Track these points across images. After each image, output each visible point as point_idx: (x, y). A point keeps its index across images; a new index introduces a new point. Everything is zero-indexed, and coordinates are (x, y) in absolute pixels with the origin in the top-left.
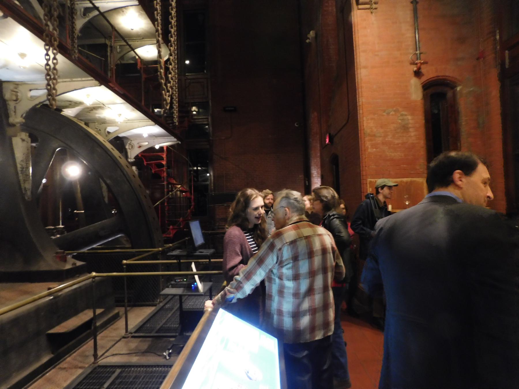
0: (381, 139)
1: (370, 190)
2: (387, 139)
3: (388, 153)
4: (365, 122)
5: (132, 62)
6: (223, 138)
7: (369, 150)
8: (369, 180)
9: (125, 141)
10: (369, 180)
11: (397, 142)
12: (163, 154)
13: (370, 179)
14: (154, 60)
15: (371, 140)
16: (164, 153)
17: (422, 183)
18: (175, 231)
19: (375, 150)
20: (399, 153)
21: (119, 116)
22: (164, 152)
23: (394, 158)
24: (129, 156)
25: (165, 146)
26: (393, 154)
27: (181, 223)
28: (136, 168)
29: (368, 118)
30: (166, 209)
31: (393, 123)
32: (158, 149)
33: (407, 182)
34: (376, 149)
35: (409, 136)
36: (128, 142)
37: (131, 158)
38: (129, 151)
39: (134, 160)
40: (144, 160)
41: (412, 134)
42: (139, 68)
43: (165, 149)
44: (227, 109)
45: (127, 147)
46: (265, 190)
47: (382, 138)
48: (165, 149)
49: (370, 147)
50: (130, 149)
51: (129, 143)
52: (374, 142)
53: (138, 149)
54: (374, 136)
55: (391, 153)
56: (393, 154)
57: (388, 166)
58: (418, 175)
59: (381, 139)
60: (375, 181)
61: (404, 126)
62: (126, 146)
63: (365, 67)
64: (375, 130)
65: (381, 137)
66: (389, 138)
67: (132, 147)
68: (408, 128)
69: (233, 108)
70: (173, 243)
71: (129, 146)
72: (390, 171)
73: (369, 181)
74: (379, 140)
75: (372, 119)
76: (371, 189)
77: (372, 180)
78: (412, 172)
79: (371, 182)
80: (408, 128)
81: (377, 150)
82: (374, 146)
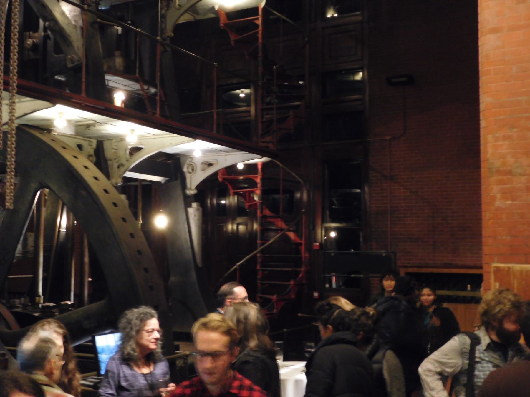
0: (523, 179)
4: (489, 145)
5: (212, 15)
6: (388, 138)
7: (498, 203)
9: (182, 159)
12: (256, 177)
13: (499, 262)
14: (240, 9)
15: (501, 182)
16: (257, 175)
19: (509, 202)
21: (132, 133)
24: (188, 185)
25: (260, 162)
28: (197, 205)
29: (497, 135)
30: (259, 277)
32: (242, 170)
34: (513, 200)
37: (190, 189)
38: (188, 176)
40: (230, 187)
42: (222, 25)
43: (259, 167)
44: (394, 80)
45: (185, 170)
46: (136, 308)
47: (526, 177)
48: (259, 167)
49: (499, 196)
50: (190, 173)
51: (188, 162)
52: (509, 186)
54: (510, 173)
59: (523, 179)
60: (507, 269)
62: (183, 168)
63: (495, 31)
64: (510, 160)
65: (523, 175)
67: (193, 170)
69: (405, 79)
70: (168, 355)
71: (188, 168)
73: (495, 267)
75: (505, 138)
76: (497, 285)
79: (498, 270)
81: (515, 202)
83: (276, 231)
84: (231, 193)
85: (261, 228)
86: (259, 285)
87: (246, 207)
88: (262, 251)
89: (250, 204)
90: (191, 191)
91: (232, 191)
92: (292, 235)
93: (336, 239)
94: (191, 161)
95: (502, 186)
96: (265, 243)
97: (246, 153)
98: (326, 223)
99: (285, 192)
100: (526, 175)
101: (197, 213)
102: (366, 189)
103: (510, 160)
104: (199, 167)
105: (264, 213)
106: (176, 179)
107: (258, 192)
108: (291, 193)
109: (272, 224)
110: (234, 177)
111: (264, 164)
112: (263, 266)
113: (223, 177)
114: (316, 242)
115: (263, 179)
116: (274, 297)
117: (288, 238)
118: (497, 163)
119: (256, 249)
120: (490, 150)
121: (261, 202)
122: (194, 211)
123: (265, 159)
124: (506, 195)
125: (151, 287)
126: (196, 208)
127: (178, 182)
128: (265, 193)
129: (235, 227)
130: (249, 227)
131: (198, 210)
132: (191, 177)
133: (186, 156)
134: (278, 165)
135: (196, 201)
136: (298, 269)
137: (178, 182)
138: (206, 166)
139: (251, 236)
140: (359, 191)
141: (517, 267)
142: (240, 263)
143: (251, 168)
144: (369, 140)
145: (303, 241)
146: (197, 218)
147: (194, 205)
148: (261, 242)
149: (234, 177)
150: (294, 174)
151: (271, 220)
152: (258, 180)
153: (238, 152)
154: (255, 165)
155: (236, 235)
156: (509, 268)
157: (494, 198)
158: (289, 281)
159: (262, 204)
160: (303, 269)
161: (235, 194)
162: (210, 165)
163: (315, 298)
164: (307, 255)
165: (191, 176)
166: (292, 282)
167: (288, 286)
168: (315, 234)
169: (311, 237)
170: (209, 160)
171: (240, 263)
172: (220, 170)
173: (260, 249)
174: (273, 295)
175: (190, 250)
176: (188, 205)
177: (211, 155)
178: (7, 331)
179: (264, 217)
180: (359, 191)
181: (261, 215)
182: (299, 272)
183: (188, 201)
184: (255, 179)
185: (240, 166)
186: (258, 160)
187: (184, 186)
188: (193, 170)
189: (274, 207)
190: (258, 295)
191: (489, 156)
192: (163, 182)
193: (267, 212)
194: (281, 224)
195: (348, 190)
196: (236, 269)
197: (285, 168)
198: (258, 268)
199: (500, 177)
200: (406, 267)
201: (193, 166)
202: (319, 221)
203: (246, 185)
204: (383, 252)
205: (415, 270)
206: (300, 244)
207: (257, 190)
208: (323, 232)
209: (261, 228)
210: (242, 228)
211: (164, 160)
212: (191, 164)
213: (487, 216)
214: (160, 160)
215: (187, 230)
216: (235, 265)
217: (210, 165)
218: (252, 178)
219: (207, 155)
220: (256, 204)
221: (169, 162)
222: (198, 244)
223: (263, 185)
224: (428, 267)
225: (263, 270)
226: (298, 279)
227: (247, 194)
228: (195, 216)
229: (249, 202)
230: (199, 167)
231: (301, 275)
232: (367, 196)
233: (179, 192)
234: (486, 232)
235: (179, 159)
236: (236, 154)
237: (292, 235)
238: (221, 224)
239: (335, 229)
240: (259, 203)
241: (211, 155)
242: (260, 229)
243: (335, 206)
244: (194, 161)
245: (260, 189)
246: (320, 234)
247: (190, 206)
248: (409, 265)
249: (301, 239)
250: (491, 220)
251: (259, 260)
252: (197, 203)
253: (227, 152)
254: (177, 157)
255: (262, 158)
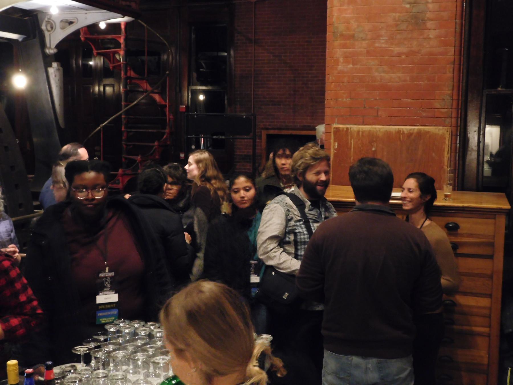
0: (364, 43)
1: (334, 145)
2: (377, 45)
3: (376, 74)
4: (335, 9)
7: (340, 67)
8: (335, 126)
10: (335, 126)
11: (397, 50)
12: (120, 37)
13: (338, 123)
15: (344, 46)
17: (443, 137)
18: (127, 179)
20: (400, 75)
22: (120, 34)
23: (390, 84)
26: (387, 76)
27: (140, 165)
30: (123, 138)
31: (394, 10)
33: (410, 134)
35: (425, 39)
36: (44, 19)
37: (50, 48)
38: (47, 34)
39: (55, 51)
41: (432, 34)
43: (123, 27)
45: (43, 27)
47: (367, 42)
48: (123, 27)
49: (341, 59)
50: (49, 31)
51: (46, 19)
53: (62, 30)
55: (382, 74)
56: (387, 76)
57: (376, 99)
58: (435, 120)
59: (364, 43)
60: (345, 129)
61: (415, 17)
62: (41, 26)
64: (354, 24)
65: (364, 40)
66: (382, 43)
67: (52, 28)
68: (424, 21)
71: (46, 26)
72: (378, 111)
73: (334, 128)
74: (361, 46)
77: (341, 126)
78: (424, 114)
79: (337, 130)
80: (424, 21)
82: (351, 58)
83: (142, 92)
84: (95, 54)
85: (125, 90)
86: (124, 146)
87: (111, 68)
88: (127, 113)
89: (114, 65)
90: (51, 50)
91: (95, 52)
92: (157, 97)
93: (206, 101)
94: (48, 19)
95: (345, 50)
96: (129, 105)
97: (107, 12)
98: (193, 85)
99: (150, 54)
100: (367, 40)
101: (58, 74)
102: (232, 52)
103: (354, 24)
104: (58, 25)
105: (128, 74)
106: (34, 37)
107: (122, 53)
108: (158, 54)
109: (139, 86)
110: (97, 36)
111: (127, 24)
112: (126, 127)
113: (86, 36)
114: (182, 104)
115: (126, 39)
116: (139, 158)
117: (154, 100)
118: (342, 27)
119: (121, 110)
120: (335, 14)
121: (124, 63)
122: (54, 71)
123: (126, 19)
124: (347, 58)
125: (6, 147)
126: (57, 68)
127: (37, 40)
128: (128, 54)
129: (102, 89)
130: (116, 88)
131: (58, 70)
132: (50, 35)
133: (44, 12)
134: (143, 26)
135: (56, 60)
136: (163, 131)
137: (37, 40)
138: (67, 24)
139: (117, 97)
140: (226, 54)
141: (355, 128)
142: (103, 125)
143: (114, 28)
144: (234, 2)
145: (167, 104)
146: (57, 78)
147: (55, 65)
148: (125, 103)
149: (97, 36)
150: (158, 35)
151: (138, 82)
152: (122, 41)
153: (98, 10)
154: (118, 25)
155: (103, 96)
156: (347, 129)
157: (337, 62)
158: (154, 142)
159: (126, 65)
160: (167, 130)
161: (99, 54)
162: (71, 23)
163: (181, 158)
164: (171, 117)
165: (50, 35)
166: (156, 143)
167: (153, 146)
168: (182, 97)
169: (177, 100)
170: (69, 17)
171: (103, 125)
172: (82, 28)
173: (124, 110)
174: (138, 155)
175: (52, 111)
176: (47, 65)
177: (70, 13)
178: (351, 211)
179: (127, 78)
180: (226, 54)
181: (125, 76)
182: (163, 134)
183: (47, 61)
184: (119, 40)
185: (103, 26)
186: (121, 20)
187: (43, 45)
188: (52, 28)
189: (139, 70)
190: (123, 156)
191: (334, 20)
192: (20, 40)
193: (132, 74)
194: (145, 86)
195: (215, 54)
196: (100, 130)
197: (150, 29)
198: (123, 129)
199: (343, 42)
200: (267, 129)
201: (52, 24)
202: (186, 84)
203: (111, 46)
204: (244, 115)
205: (276, 132)
206: (165, 106)
207: (121, 50)
208: (190, 94)
209: (125, 90)
210: (109, 90)
211: (21, 16)
212: (50, 22)
213: (330, 79)
214: (16, 16)
215: (48, 90)
216: (99, 126)
217: (71, 23)
218: (115, 38)
219: (66, 13)
220: (120, 65)
221: (26, 18)
222: (60, 105)
223: (126, 46)
224: (288, 129)
225: (128, 132)
226: (162, 140)
227: (111, 55)
228: (55, 76)
229: (114, 63)
230: (58, 25)
231: (165, 137)
232: (232, 60)
233: (39, 51)
234: (328, 95)
235: (36, 16)
236: (96, 13)
237: (157, 97)
238: (87, 86)
239: (204, 92)
240: (123, 63)
241: (70, 13)
242: (124, 91)
243: (203, 68)
244: (52, 18)
245: (123, 50)
246: (187, 96)
247: (51, 66)
248: (270, 127)
249: (165, 101)
250: (333, 83)
251: (124, 121)
252: (58, 62)
253: (86, 10)
254: (35, 13)
255: (123, 17)
